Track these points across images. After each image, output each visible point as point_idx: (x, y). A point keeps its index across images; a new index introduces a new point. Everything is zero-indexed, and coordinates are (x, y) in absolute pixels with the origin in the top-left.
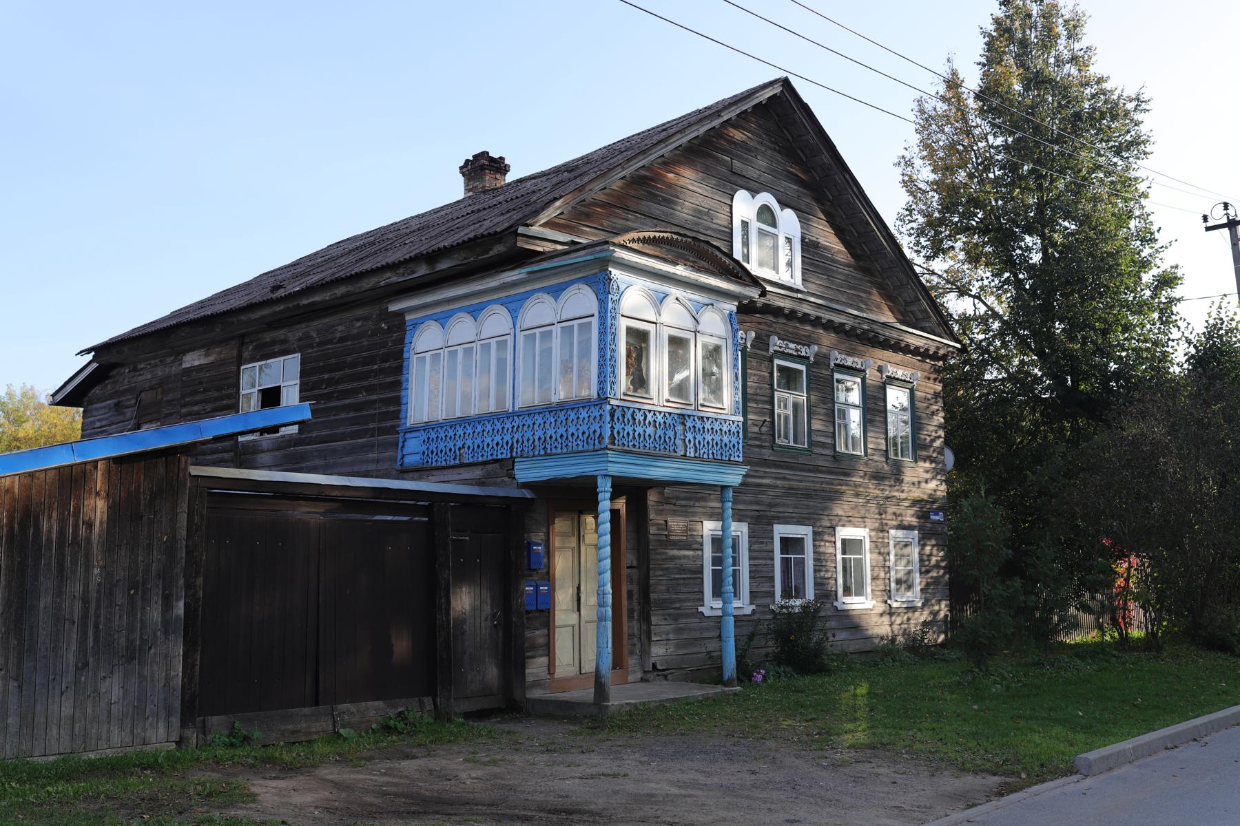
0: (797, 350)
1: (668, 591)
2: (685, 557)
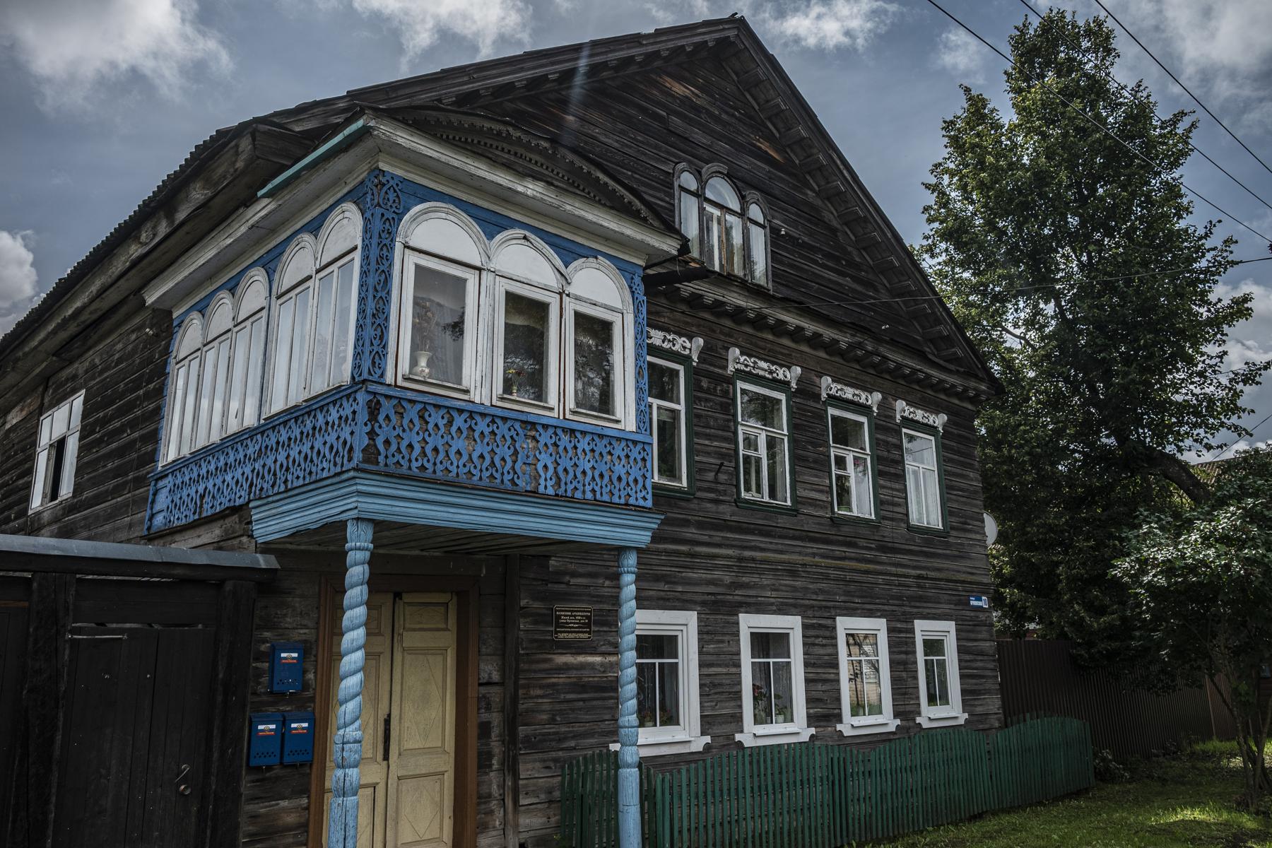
0: (771, 372)
1: (552, 721)
2: (582, 666)
